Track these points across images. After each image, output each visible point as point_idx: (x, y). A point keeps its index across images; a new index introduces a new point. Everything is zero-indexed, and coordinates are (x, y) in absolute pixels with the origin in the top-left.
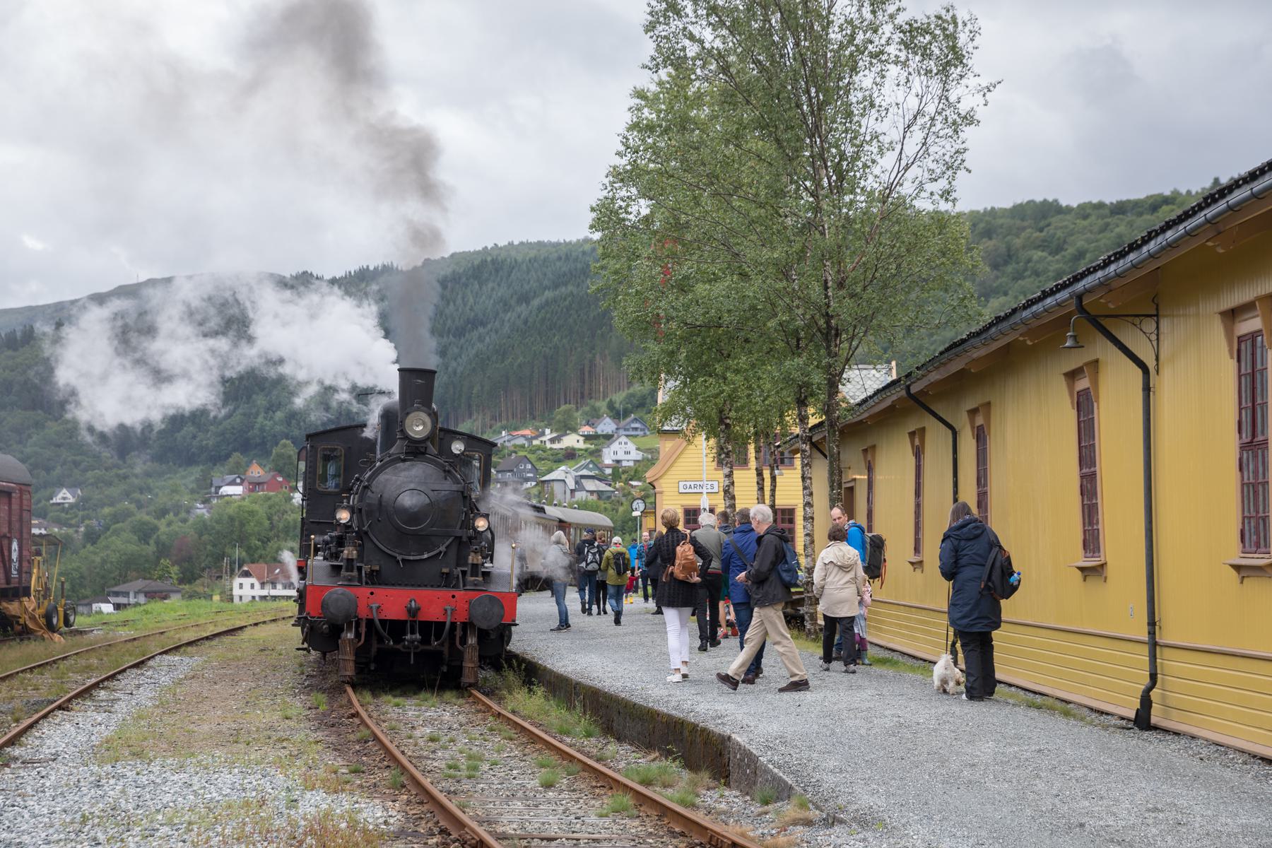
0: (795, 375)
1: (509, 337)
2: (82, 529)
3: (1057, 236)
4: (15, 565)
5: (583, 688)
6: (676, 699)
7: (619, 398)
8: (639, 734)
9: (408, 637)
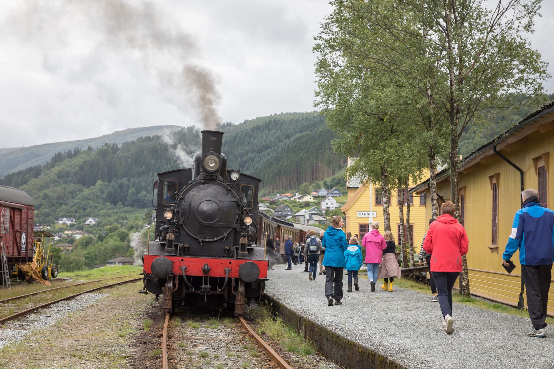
0: (429, 140)
1: (281, 153)
2: (97, 235)
3: (525, 109)
4: (23, 246)
5: (305, 321)
6: (367, 333)
7: (329, 180)
8: (341, 356)
9: (203, 286)
